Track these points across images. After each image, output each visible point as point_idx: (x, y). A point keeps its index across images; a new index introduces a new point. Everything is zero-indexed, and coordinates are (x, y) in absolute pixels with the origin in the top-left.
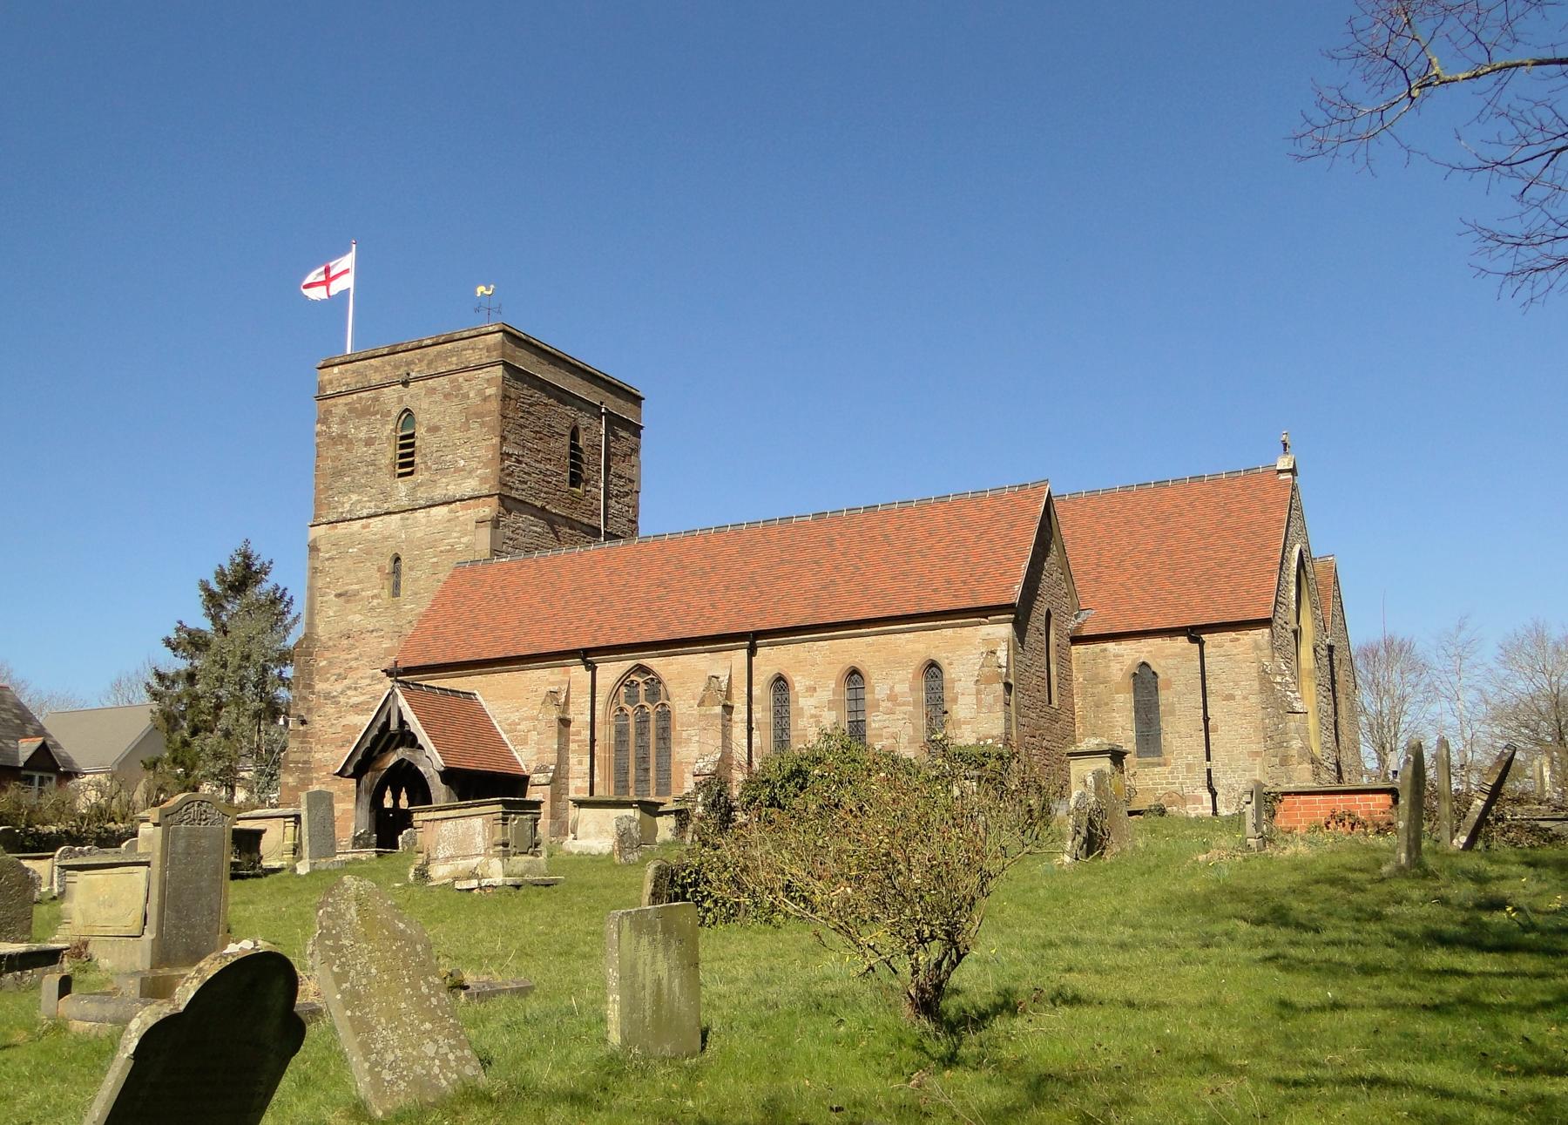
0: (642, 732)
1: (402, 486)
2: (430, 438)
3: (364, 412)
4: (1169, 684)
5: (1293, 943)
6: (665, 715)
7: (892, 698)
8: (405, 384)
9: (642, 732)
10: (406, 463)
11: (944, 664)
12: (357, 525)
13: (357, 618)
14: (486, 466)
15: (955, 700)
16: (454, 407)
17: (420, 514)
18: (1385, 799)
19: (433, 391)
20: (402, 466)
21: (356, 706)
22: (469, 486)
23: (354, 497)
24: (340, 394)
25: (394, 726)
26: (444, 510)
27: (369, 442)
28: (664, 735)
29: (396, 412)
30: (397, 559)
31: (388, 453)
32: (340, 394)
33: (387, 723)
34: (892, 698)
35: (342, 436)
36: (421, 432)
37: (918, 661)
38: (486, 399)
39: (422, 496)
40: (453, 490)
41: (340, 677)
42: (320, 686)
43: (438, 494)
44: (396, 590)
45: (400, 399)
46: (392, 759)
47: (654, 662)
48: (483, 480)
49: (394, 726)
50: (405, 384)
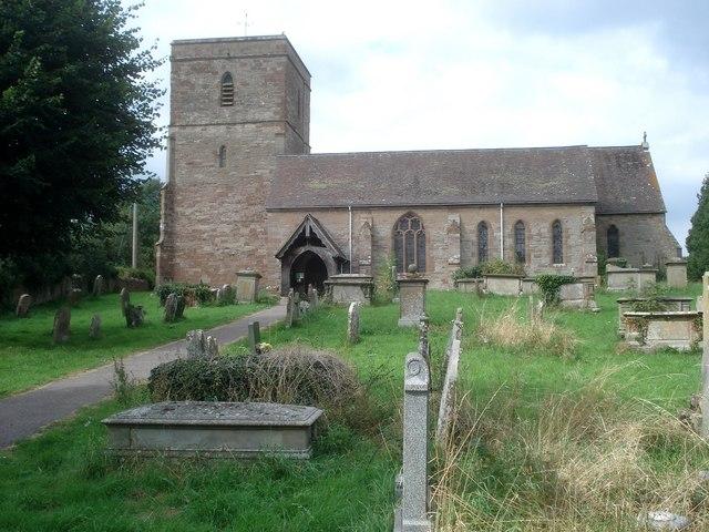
0: (409, 243)
1: (226, 112)
2: (243, 88)
3: (199, 70)
4: (623, 234)
5: (443, 422)
6: (422, 236)
7: (539, 234)
9: (409, 243)
10: (228, 97)
12: (198, 129)
15: (568, 237)
17: (238, 127)
20: (225, 101)
22: (268, 115)
23: (196, 114)
24: (185, 60)
25: (308, 234)
26: (254, 126)
27: (205, 87)
28: (421, 246)
29: (221, 73)
31: (217, 95)
32: (185, 60)
33: (304, 231)
34: (539, 234)
36: (237, 84)
37: (551, 220)
38: (277, 73)
39: (239, 118)
40: (258, 117)
41: (190, 206)
42: (179, 209)
43: (249, 117)
46: (302, 250)
48: (275, 113)
49: (308, 234)
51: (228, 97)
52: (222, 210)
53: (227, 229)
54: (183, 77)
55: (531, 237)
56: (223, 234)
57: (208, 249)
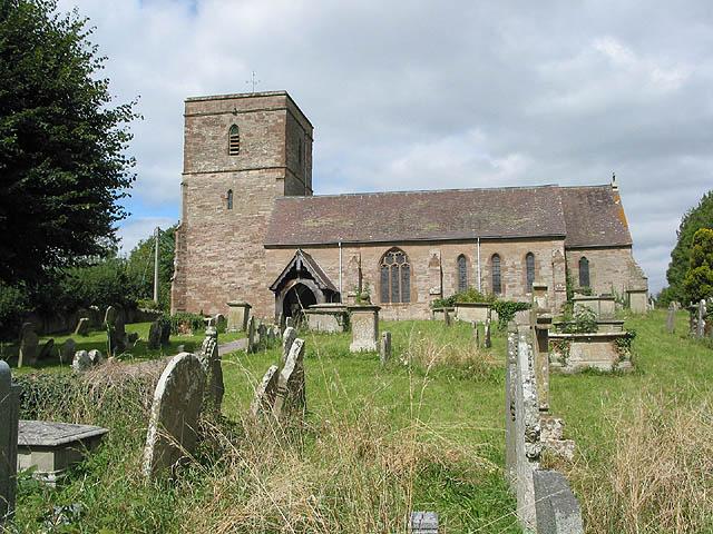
3: (211, 124)
4: (593, 265)
6: (406, 268)
8: (235, 113)
10: (234, 146)
11: (536, 254)
13: (210, 218)
14: (279, 153)
16: (261, 126)
18: (117, 195)
19: (250, 118)
21: (209, 258)
22: (269, 163)
23: (207, 163)
25: (298, 268)
28: (406, 278)
30: (230, 191)
31: (225, 146)
35: (199, 135)
36: (243, 137)
37: (525, 253)
38: (278, 124)
40: (260, 164)
43: (253, 165)
44: (230, 206)
45: (231, 120)
47: (403, 248)
49: (298, 268)
50: (235, 113)
51: (234, 146)
52: (229, 248)
53: (232, 265)
54: (195, 131)
55: (506, 269)
56: (230, 270)
57: (216, 282)
